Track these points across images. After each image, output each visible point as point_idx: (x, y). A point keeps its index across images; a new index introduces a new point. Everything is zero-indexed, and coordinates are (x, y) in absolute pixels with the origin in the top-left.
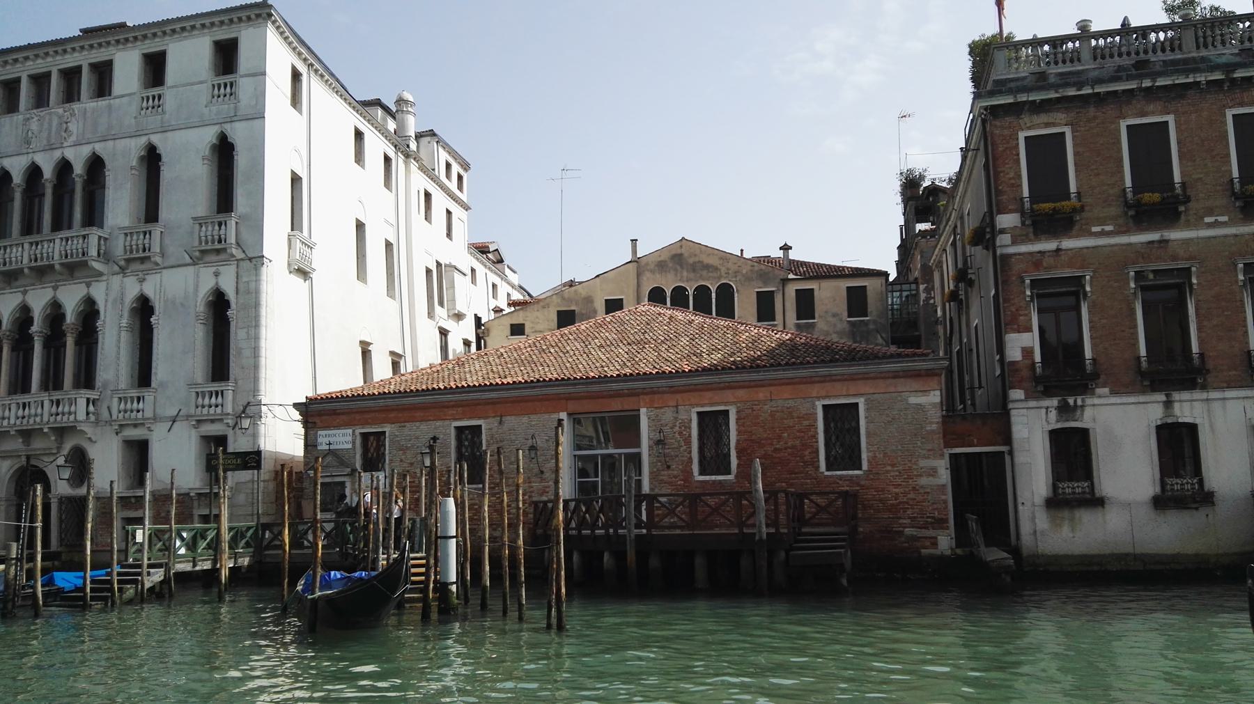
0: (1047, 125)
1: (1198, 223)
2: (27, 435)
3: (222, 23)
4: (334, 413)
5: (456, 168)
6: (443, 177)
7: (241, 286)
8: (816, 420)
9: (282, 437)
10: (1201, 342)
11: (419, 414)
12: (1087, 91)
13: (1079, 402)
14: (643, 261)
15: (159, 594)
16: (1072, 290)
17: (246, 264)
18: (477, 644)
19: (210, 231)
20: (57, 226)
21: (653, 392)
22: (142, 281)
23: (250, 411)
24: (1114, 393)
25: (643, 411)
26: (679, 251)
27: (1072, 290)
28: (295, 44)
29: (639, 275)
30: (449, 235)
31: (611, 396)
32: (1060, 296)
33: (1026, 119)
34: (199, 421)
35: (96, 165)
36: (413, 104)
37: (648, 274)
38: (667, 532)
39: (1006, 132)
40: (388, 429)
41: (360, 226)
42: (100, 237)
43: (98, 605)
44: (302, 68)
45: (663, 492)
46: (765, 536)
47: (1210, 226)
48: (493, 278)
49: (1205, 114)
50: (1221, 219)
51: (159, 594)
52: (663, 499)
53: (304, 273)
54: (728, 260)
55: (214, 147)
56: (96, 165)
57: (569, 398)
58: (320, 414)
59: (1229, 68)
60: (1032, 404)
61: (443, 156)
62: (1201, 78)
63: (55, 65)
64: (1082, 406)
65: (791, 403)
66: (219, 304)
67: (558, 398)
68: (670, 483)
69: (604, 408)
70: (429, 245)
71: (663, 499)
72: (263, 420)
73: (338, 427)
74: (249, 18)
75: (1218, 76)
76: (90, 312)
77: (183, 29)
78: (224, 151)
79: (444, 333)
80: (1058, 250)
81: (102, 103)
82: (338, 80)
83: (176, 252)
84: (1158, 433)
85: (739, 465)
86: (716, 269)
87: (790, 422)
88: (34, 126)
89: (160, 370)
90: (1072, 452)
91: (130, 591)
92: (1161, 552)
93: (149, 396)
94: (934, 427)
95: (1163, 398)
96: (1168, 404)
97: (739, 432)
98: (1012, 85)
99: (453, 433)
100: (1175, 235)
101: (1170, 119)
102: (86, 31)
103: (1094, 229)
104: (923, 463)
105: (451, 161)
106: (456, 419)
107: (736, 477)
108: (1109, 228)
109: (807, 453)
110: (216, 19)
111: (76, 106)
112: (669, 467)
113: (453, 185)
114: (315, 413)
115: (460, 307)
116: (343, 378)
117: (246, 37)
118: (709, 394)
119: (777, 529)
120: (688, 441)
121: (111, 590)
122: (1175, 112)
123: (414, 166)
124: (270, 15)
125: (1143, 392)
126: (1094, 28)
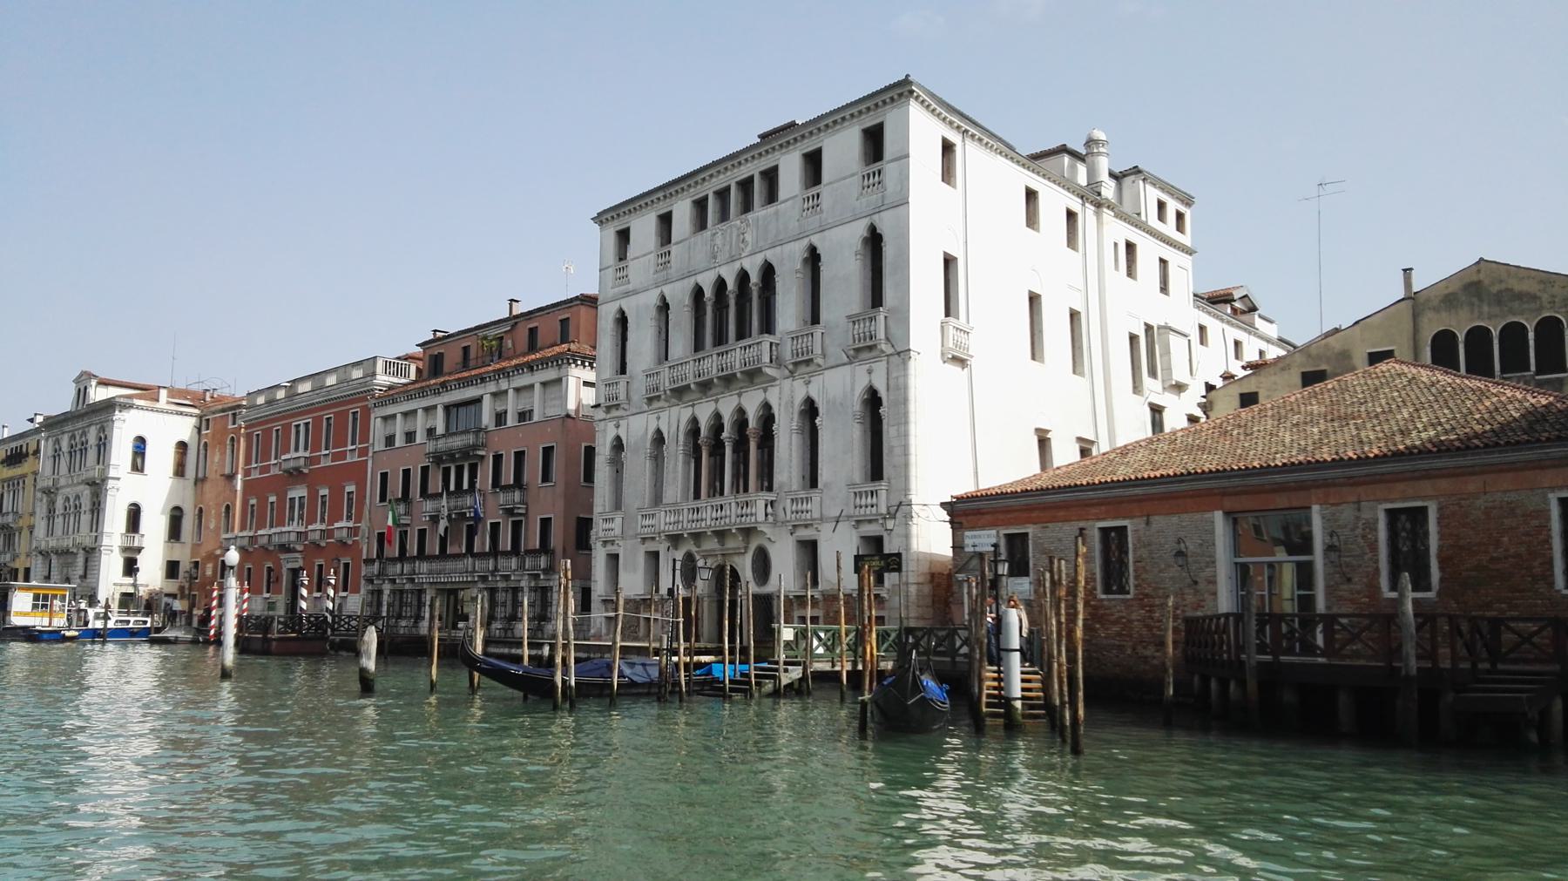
2: (721, 535)
3: (868, 109)
4: (979, 512)
5: (1172, 206)
6: (1153, 221)
7: (892, 383)
8: (1548, 519)
9: (931, 537)
11: (1061, 513)
14: (1421, 299)
15: (797, 690)
18: (314, 674)
19: (860, 328)
20: (741, 335)
21: (1326, 484)
22: (808, 383)
23: (901, 509)
25: (1315, 508)
26: (1475, 278)
28: (945, 114)
29: (1415, 316)
30: (1164, 289)
31: (1274, 491)
34: (858, 522)
35: (768, 271)
36: (1104, 143)
37: (1429, 315)
38: (1348, 662)
40: (1030, 530)
41: (1034, 299)
43: (737, 697)
44: (954, 137)
45: (1344, 610)
46: (1414, 672)
48: (1234, 333)
51: (797, 690)
52: (1344, 621)
53: (960, 361)
54: (1552, 284)
55: (866, 240)
56: (768, 271)
57: (1224, 493)
58: (966, 513)
61: (1152, 195)
63: (732, 178)
65: (1513, 496)
66: (873, 400)
67: (1209, 493)
68: (1352, 601)
69: (1264, 501)
70: (1133, 303)
71: (1344, 621)
72: (915, 520)
73: (983, 527)
74: (892, 99)
76: (768, 418)
77: (835, 122)
78: (874, 241)
79: (1156, 410)
81: (771, 209)
82: (1000, 140)
83: (836, 353)
85: (1442, 580)
86: (1534, 298)
88: (719, 240)
89: (824, 474)
91: (769, 686)
93: (815, 496)
97: (1442, 536)
99: (1097, 535)
102: (763, 137)
106: (1099, 519)
107: (1439, 594)
109: (1536, 564)
110: (863, 107)
111: (750, 216)
112: (1349, 580)
113: (1169, 228)
114: (963, 512)
115: (1180, 374)
116: (1012, 467)
117: (890, 119)
118: (1400, 486)
119: (1474, 665)
120: (1373, 547)
121: (749, 683)
123: (1107, 215)
124: (912, 92)
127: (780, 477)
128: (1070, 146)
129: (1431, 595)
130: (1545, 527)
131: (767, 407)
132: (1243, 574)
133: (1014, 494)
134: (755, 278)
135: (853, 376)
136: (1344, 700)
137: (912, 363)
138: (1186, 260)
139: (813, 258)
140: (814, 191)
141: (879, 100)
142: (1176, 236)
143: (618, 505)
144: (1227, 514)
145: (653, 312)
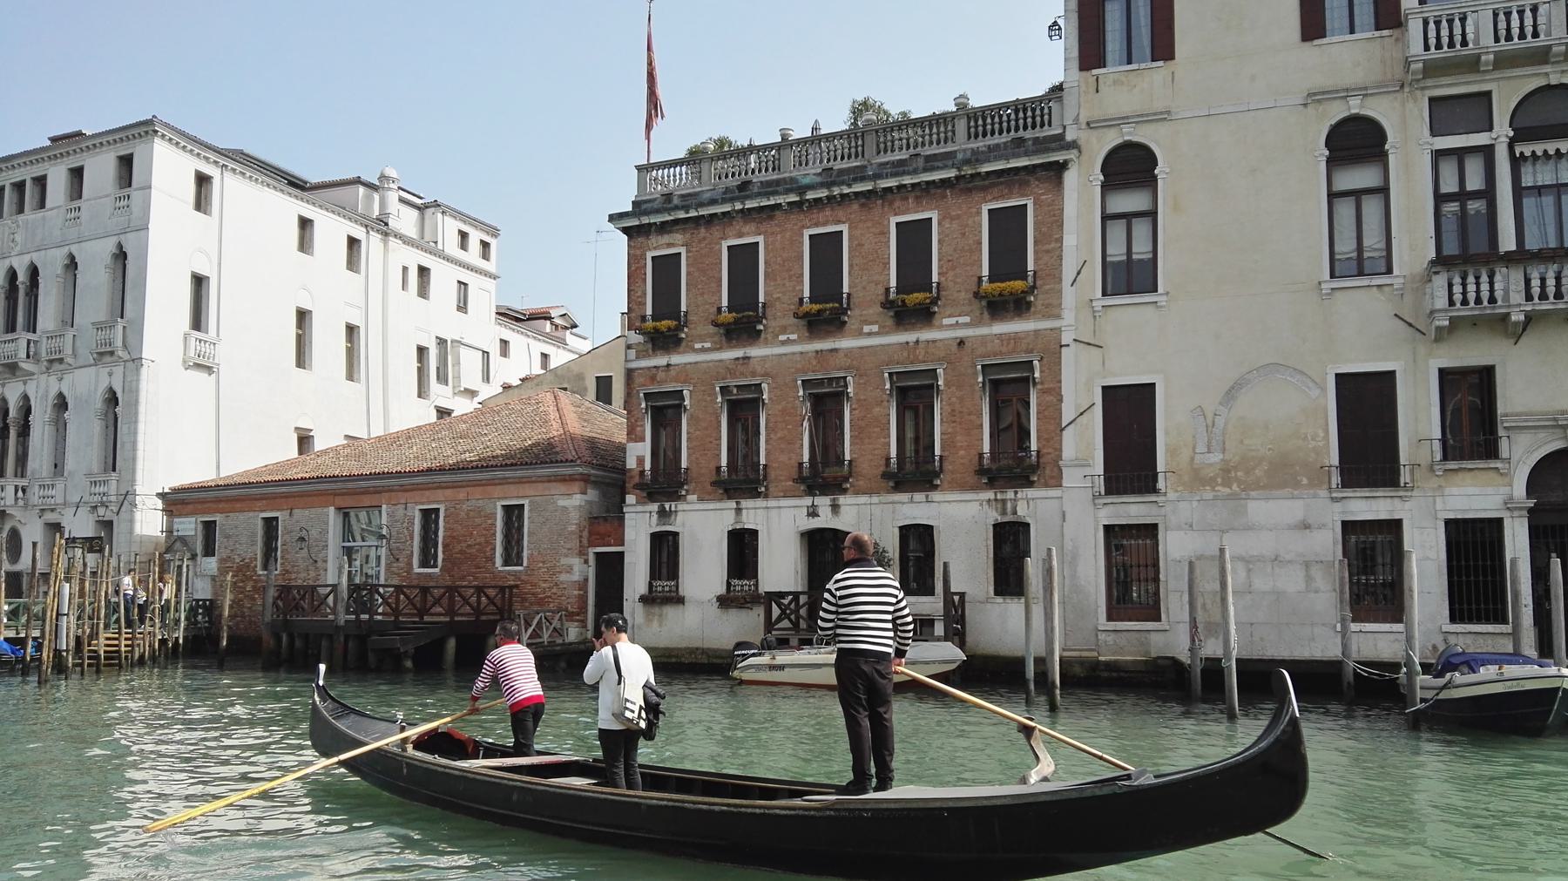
1: (774, 341)
5: (475, 236)
12: (693, 214)
17: (130, 364)
21: (390, 490)
22: (61, 380)
23: (127, 498)
24: (701, 499)
33: (654, 240)
35: (34, 272)
40: (218, 518)
41: (303, 316)
42: (29, 342)
47: (783, 343)
49: (788, 234)
50: (962, 320)
56: (34, 272)
60: (640, 508)
62: (780, 200)
66: (112, 399)
73: (186, 515)
78: (121, 256)
80: (668, 365)
81: (40, 214)
83: (86, 356)
89: (70, 464)
95: (734, 505)
96: (738, 510)
99: (260, 524)
100: (755, 352)
101: (683, 250)
102: (54, 140)
103: (698, 346)
104: (564, 561)
105: (465, 228)
111: (21, 217)
113: (473, 255)
114: (176, 502)
117: (138, 151)
121: (119, 658)
122: (765, 233)
125: (721, 500)
127: (32, 464)
128: (364, 178)
129: (437, 570)
131: (26, 398)
133: (227, 487)
134: (22, 277)
135: (97, 375)
137: (144, 371)
139: (72, 264)
140: (76, 204)
141: (129, 133)
142: (482, 264)
143: (58, 467)
144: (339, 509)
145: (108, 259)
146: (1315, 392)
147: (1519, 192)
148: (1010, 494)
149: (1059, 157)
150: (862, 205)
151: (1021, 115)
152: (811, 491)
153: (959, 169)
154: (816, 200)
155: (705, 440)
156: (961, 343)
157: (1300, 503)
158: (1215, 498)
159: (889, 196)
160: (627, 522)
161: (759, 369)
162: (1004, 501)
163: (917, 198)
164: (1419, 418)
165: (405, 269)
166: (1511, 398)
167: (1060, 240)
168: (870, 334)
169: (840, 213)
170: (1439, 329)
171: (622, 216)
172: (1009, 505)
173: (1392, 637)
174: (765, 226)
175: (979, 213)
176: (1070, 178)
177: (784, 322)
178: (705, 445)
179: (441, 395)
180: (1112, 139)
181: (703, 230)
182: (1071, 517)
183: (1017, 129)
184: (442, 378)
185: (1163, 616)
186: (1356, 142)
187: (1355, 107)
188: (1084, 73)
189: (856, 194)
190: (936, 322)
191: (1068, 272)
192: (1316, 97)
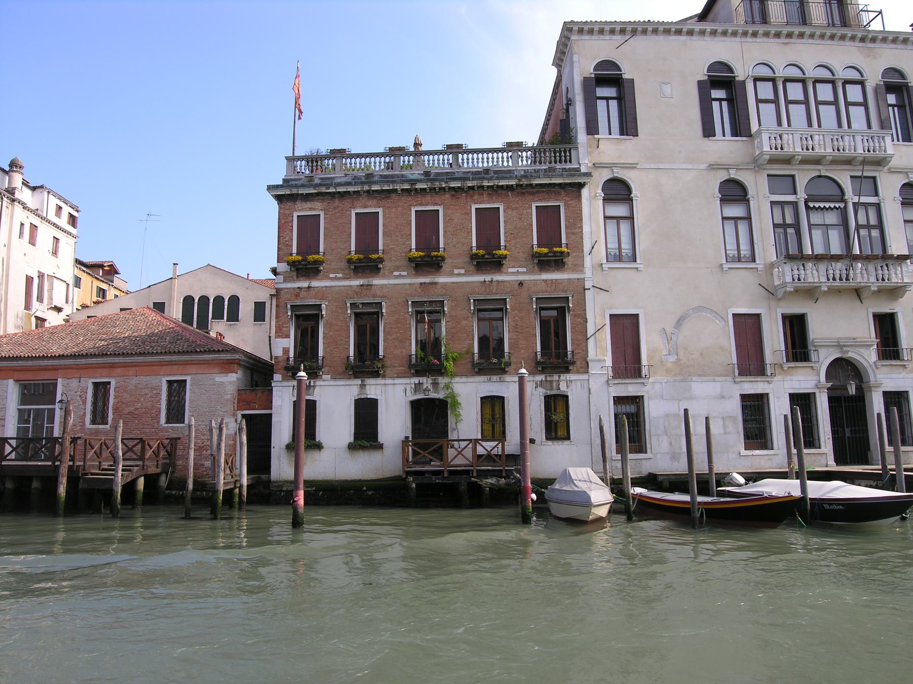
0: (311, 209)
1: (390, 275)
5: (66, 210)
6: (52, 216)
10: (385, 349)
12: (332, 190)
13: (312, 384)
16: (499, 307)
24: (333, 378)
25: (60, 380)
27: (499, 307)
32: (490, 309)
33: (299, 205)
39: (287, 212)
50: (521, 270)
59: (413, 182)
60: (285, 384)
61: (54, 201)
64: (314, 386)
75: (406, 186)
80: (309, 287)
84: (355, 404)
87: (146, 391)
90: (306, 415)
92: (316, 479)
94: (229, 397)
96: (363, 386)
98: (293, 183)
103: (332, 276)
105: (61, 204)
108: (340, 275)
113: (63, 222)
122: (383, 207)
126: (423, 148)
129: (107, 426)
130: (159, 394)
132: (23, 417)
136: (35, 484)
138: (72, 241)
146: (722, 324)
147: (810, 226)
148: (556, 377)
149: (581, 180)
150: (453, 196)
151: (563, 154)
152: (418, 373)
153: (520, 180)
154: (422, 189)
155: (337, 338)
156: (521, 284)
157: (718, 384)
158: (675, 381)
159: (471, 192)
160: (274, 393)
161: (378, 293)
162: (551, 382)
163: (489, 194)
164: (774, 339)
165: (22, 224)
166: (816, 330)
167: (581, 228)
168: (459, 275)
169: (437, 199)
170: (785, 292)
171: (277, 187)
172: (555, 384)
173: (766, 457)
174: (384, 202)
175: (530, 207)
176: (585, 192)
177: (397, 263)
178: (335, 342)
179: (40, 310)
180: (606, 175)
181: (337, 201)
182: (592, 393)
183: (550, 163)
184: (40, 299)
185: (648, 450)
186: (733, 192)
187: (734, 174)
188: (590, 137)
189: (450, 188)
190: (504, 269)
191: (587, 247)
192: (714, 167)
